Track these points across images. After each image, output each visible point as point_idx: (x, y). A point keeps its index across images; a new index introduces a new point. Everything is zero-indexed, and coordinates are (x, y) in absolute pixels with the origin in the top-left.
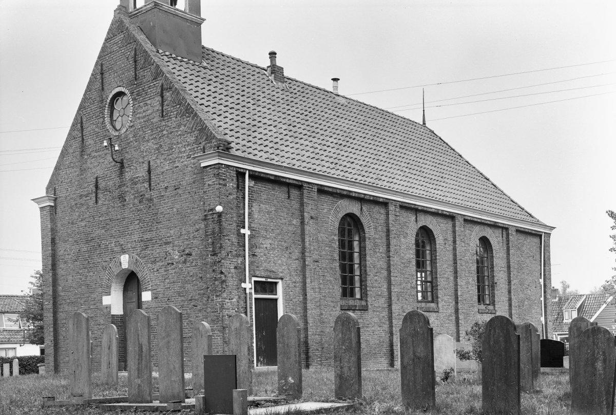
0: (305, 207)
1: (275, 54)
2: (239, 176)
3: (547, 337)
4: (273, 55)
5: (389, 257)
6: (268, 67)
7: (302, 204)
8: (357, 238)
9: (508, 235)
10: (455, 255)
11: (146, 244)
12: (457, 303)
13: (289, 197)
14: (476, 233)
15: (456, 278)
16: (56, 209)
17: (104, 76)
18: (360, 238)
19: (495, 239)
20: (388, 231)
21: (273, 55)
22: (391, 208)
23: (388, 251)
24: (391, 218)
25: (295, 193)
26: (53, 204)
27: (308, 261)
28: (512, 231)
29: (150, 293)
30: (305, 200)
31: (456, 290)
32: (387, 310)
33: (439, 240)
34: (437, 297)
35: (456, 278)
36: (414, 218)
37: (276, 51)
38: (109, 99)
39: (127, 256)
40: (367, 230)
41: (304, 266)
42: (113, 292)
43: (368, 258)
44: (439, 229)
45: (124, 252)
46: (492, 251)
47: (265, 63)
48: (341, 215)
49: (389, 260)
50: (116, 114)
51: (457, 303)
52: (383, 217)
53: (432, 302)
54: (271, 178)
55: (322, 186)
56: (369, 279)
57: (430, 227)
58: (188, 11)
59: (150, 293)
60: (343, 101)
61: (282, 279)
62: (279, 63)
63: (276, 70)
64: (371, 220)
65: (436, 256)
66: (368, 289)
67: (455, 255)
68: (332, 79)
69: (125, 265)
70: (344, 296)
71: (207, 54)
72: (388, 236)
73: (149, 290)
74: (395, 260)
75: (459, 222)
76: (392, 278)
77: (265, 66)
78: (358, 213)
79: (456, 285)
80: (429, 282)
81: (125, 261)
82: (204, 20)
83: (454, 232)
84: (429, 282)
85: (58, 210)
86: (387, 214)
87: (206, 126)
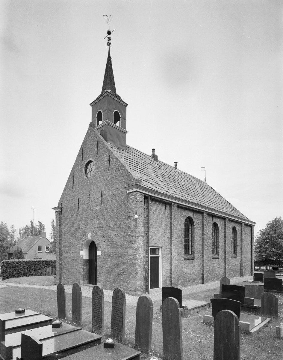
0: (172, 214)
1: (155, 150)
2: (145, 199)
3: (276, 275)
4: (153, 150)
5: (203, 236)
6: (151, 155)
7: (171, 212)
8: (190, 228)
9: (242, 226)
10: (225, 234)
11: (99, 229)
12: (225, 254)
13: (166, 209)
14: (231, 225)
15: (225, 244)
16: (61, 213)
17: (83, 154)
18: (192, 228)
19: (238, 228)
20: (203, 224)
21: (153, 150)
22: (204, 214)
23: (203, 233)
24: (204, 218)
25: (168, 208)
26: (60, 210)
27: (173, 238)
28: (243, 225)
29: (101, 251)
30: (173, 210)
31: (225, 249)
32: (201, 259)
33: (220, 228)
34: (218, 252)
35: (225, 244)
36: (211, 219)
37: (155, 149)
38: (85, 164)
39: (91, 234)
40: (195, 224)
41: (171, 241)
42: (54, 333)
43: (195, 236)
44: (220, 223)
45: (89, 232)
46: (236, 232)
47: (150, 153)
48: (185, 217)
49: (203, 237)
50: (88, 170)
51: (225, 254)
52: (201, 218)
53: (216, 254)
54: (159, 199)
55: (179, 204)
56: (195, 245)
57: (217, 223)
58: (121, 127)
59: (101, 251)
60: (179, 171)
61: (162, 247)
62: (156, 153)
63: (155, 157)
64: (196, 219)
65: (218, 235)
66: (195, 250)
67: (225, 234)
68: (175, 163)
69: (90, 238)
70: (186, 253)
71: (128, 148)
72: (203, 226)
73: (100, 250)
74: (205, 237)
75: (227, 220)
76: (204, 245)
77: (150, 155)
78: (192, 216)
79: (225, 247)
80: (215, 246)
81: (90, 236)
82: (127, 132)
83: (225, 225)
84: (215, 246)
85: (63, 213)
86: (203, 217)
87: (130, 174)
